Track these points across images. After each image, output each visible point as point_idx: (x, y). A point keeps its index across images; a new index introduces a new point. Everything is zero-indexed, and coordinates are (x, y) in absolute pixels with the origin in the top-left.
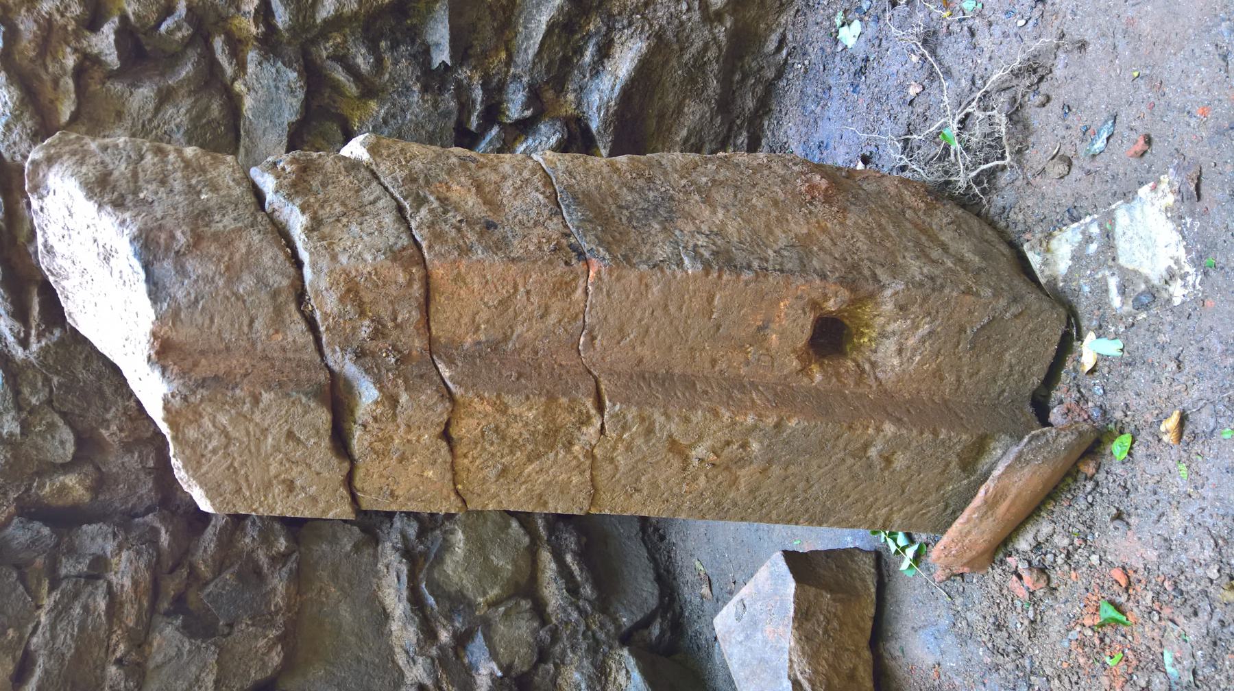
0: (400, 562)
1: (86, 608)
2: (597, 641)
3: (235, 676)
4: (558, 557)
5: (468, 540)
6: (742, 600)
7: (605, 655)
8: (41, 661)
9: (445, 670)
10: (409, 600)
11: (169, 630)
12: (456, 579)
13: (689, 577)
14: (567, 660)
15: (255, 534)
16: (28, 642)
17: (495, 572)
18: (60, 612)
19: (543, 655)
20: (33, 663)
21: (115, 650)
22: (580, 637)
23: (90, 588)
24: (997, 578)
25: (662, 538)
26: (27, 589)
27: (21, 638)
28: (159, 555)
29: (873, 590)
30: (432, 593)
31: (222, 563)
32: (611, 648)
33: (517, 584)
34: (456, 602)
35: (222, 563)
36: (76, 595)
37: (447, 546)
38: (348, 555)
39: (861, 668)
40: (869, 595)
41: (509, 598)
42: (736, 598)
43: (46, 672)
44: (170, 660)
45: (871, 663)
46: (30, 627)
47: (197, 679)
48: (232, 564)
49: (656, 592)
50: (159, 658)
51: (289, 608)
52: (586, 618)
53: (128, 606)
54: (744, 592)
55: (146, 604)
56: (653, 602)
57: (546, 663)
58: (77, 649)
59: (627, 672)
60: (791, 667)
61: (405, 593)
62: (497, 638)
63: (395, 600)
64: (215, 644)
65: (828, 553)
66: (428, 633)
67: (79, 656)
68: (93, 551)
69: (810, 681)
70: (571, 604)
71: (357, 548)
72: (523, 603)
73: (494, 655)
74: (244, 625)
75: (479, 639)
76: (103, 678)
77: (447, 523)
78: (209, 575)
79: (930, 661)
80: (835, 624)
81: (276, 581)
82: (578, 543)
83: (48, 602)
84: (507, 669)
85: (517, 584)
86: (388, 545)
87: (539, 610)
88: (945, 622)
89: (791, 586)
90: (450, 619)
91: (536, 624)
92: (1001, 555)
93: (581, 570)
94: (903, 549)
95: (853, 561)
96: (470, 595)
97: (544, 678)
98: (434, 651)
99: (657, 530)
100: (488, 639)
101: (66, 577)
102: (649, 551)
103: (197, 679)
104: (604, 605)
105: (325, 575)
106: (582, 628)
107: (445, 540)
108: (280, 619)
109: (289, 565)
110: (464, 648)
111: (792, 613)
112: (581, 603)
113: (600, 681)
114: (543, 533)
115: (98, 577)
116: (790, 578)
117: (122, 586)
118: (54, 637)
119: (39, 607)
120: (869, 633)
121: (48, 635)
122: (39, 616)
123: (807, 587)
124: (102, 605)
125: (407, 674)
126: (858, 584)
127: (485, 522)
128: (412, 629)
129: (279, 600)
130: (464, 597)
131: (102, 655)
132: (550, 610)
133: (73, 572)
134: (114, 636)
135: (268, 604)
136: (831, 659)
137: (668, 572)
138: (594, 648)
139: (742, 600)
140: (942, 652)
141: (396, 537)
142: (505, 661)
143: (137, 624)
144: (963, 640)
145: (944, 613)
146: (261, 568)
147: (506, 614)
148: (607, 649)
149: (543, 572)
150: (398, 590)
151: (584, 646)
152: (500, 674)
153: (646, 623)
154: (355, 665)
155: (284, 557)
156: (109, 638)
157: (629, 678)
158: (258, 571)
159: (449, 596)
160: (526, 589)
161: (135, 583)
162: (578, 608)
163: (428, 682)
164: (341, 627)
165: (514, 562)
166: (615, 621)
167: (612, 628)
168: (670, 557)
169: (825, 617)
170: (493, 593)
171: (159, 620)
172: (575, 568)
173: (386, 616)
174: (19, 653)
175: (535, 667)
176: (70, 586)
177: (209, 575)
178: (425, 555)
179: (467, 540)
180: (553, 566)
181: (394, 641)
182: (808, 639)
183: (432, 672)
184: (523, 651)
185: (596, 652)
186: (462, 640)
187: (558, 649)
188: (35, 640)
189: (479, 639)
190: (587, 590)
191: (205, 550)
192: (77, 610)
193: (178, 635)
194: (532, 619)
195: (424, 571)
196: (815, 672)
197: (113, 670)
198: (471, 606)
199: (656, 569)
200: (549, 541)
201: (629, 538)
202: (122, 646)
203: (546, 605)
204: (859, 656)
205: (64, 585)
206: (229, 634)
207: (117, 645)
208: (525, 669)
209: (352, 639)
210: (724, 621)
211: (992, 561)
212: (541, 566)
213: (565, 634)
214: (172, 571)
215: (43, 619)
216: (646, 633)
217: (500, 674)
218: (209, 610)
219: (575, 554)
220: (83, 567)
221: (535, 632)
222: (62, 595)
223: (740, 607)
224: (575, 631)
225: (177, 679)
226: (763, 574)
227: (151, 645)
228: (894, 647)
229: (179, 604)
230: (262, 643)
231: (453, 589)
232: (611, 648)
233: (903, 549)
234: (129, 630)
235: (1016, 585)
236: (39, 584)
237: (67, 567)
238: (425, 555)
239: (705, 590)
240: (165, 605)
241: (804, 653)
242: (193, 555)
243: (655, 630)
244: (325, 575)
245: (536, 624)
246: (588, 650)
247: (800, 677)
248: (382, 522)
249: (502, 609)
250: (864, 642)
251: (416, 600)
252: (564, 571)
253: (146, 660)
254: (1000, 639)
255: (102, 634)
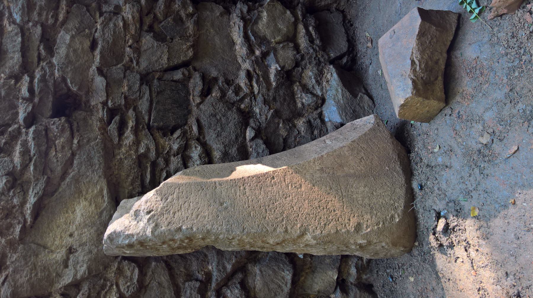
0: (240, 21)
1: (115, 25)
2: (320, 62)
3: (175, 57)
4: (306, 28)
5: (268, 15)
6: (394, 30)
7: (323, 67)
8: (100, 42)
9: (257, 65)
10: (244, 37)
11: (148, 37)
12: (263, 31)
13: (362, 40)
14: (307, 67)
15: (180, 4)
16: (94, 35)
17: (279, 30)
18: (105, 25)
19: (297, 64)
20: (97, 44)
21: (128, 42)
22: (313, 59)
23: (115, 17)
24: (519, 15)
25: (352, 25)
26: (91, 15)
27: (91, 33)
28: (141, 8)
29: (454, 29)
30: (253, 35)
31: (167, 15)
32: (325, 64)
33: (288, 37)
34: (263, 40)
35: (167, 15)
36: (110, 20)
37: (259, 18)
38: (218, 17)
39: (441, 60)
40: (452, 31)
41: (284, 41)
42: (392, 29)
43: (103, 46)
44: (149, 49)
45: (446, 58)
46: (94, 30)
47: (161, 57)
48: (171, 16)
49: (347, 46)
50: (145, 47)
51: (195, 36)
52: (316, 53)
53: (131, 26)
54: (396, 26)
55: (138, 26)
56: (345, 49)
57: (298, 67)
58: (114, 40)
59: (331, 74)
60: (412, 55)
61: (242, 34)
62: (279, 56)
63: (237, 37)
64: (166, 44)
65: (438, 12)
66: (251, 51)
67: (115, 42)
68: (114, 3)
69: (419, 61)
70: (310, 46)
71: (222, 15)
72: (290, 44)
73: (277, 62)
74: (177, 39)
75: (272, 55)
76: (124, 52)
77: (260, 8)
78: (162, 19)
79: (474, 56)
80: (435, 40)
81: (189, 24)
82: (315, 23)
83: (100, 21)
84: (283, 68)
85: (288, 37)
86: (235, 15)
87: (297, 47)
88: (486, 39)
89: (419, 20)
90: (261, 47)
91: (295, 53)
92: (524, 4)
93: (316, 33)
94: (474, 9)
95: (448, 16)
96: (268, 37)
97: (297, 73)
98: (253, 58)
99: (350, 22)
100: (275, 55)
101: (105, 12)
102: (345, 30)
103: (161, 57)
104: (325, 47)
105: (209, 24)
106: (314, 56)
107: (259, 15)
108: (191, 39)
109: (194, 18)
110: (265, 58)
111: (417, 33)
112: (314, 46)
113: (320, 76)
114: (300, 17)
115: (118, 14)
116: (419, 17)
117: (128, 18)
118: (104, 34)
119: (96, 22)
120: (448, 47)
121: (101, 33)
122: (97, 26)
123: (426, 23)
124: (121, 24)
125: (242, 66)
126: (448, 26)
127: (276, 10)
128: (244, 49)
129: (190, 31)
130: (266, 39)
131: (123, 43)
132: (301, 48)
133: (108, 10)
134: (127, 37)
135: (186, 33)
136: (429, 54)
137: (353, 38)
138: (319, 63)
139: (394, 30)
140: (481, 52)
141: (238, 11)
142: (282, 65)
143: (135, 33)
144: (493, 45)
145: (487, 36)
146: (183, 19)
147: (283, 47)
148: (324, 65)
149: (299, 33)
150: (239, 33)
151: (314, 62)
152: (279, 69)
153: (341, 57)
154: (221, 60)
155: (191, 15)
156: (125, 37)
157: (332, 76)
158: (181, 19)
159: (260, 38)
160: (291, 39)
161: (133, 17)
162: (313, 48)
163: (251, 69)
164: (215, 46)
165: (287, 27)
166: (328, 55)
167: (327, 57)
168: (354, 33)
169: (431, 36)
170: (278, 38)
171: (144, 34)
172: (313, 33)
173: (233, 43)
174: (91, 39)
175: (294, 68)
176: (107, 15)
177: (162, 19)
178: (250, 20)
179: (268, 15)
180: (304, 31)
181: (237, 53)
182: (422, 45)
183: (252, 66)
184: (289, 62)
185: (319, 65)
186: (265, 55)
187: (303, 63)
188: (96, 34)
189: (272, 55)
190: (318, 42)
191: (160, 8)
192: (111, 25)
193: (152, 40)
194: (294, 50)
195: (250, 26)
196: (422, 58)
197: (128, 49)
198: (269, 42)
199: (348, 37)
200: (302, 21)
201: (337, 24)
202: (130, 41)
203: (300, 46)
204: (442, 55)
205: (105, 14)
206: (171, 42)
207: (128, 40)
208: (290, 68)
209: (220, 51)
210: (383, 41)
211: (519, 7)
212: (298, 31)
213: (307, 58)
214: (147, 15)
215: (99, 27)
216: (340, 61)
217: (279, 69)
218: (163, 32)
219: (314, 27)
220: (112, 8)
221: (294, 56)
222: (105, 19)
223: (393, 33)
224: (311, 57)
225: (153, 56)
226: (406, 18)
227: (142, 42)
228: (458, 53)
229: (151, 29)
230: (184, 47)
231: (262, 35)
232: (325, 64)
233: (474, 9)
234: (132, 35)
235: (528, 17)
236: (95, 13)
237: (105, 8)
238: (250, 20)
239: (369, 44)
240: (145, 28)
241: (419, 50)
242: (155, 9)
243: (345, 60)
244: (209, 24)
245: (295, 53)
246: (316, 64)
247: (415, 59)
248: (232, 6)
249: (281, 45)
250: (445, 49)
251: (246, 37)
252: (308, 32)
253: (140, 47)
254: (512, 42)
255: (122, 34)
